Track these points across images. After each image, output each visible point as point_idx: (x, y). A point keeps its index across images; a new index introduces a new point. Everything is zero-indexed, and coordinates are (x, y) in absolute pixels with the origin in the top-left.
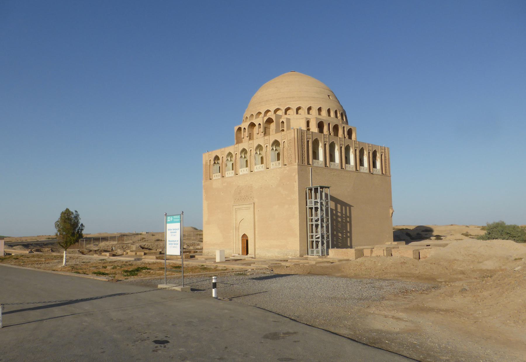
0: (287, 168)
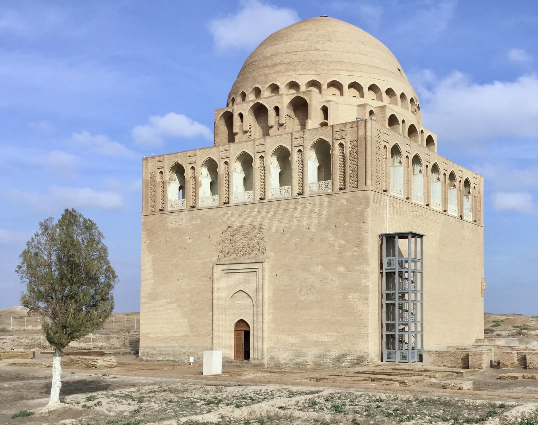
0: (346, 196)
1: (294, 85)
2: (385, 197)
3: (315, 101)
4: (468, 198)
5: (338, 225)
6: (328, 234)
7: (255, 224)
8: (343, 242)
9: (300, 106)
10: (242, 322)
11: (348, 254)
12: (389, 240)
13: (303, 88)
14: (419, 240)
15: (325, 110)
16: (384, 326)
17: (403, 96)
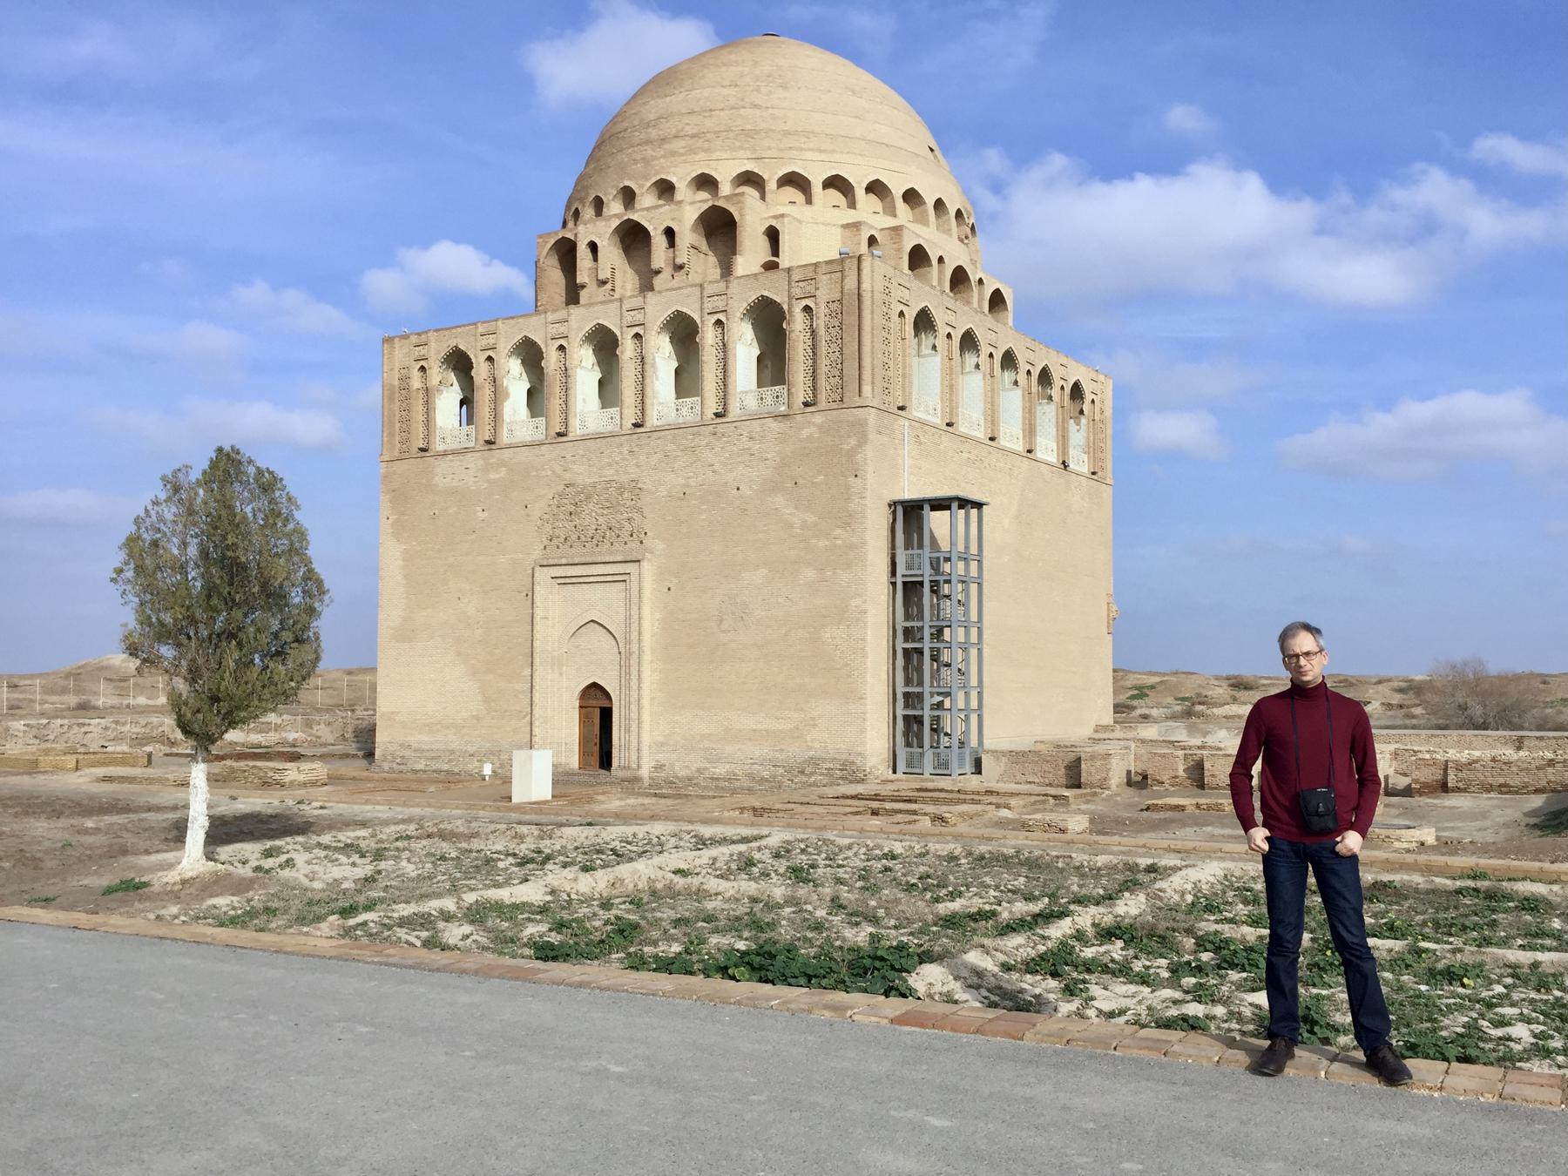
0: (819, 419)
1: (705, 182)
2: (901, 421)
3: (752, 216)
4: (1078, 424)
5: (800, 481)
6: (779, 500)
7: (624, 479)
8: (811, 518)
9: (720, 228)
10: (594, 691)
11: (822, 543)
12: (911, 513)
13: (725, 189)
14: (974, 512)
15: (773, 235)
16: (900, 696)
17: (939, 204)
